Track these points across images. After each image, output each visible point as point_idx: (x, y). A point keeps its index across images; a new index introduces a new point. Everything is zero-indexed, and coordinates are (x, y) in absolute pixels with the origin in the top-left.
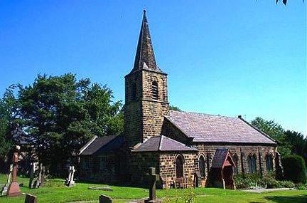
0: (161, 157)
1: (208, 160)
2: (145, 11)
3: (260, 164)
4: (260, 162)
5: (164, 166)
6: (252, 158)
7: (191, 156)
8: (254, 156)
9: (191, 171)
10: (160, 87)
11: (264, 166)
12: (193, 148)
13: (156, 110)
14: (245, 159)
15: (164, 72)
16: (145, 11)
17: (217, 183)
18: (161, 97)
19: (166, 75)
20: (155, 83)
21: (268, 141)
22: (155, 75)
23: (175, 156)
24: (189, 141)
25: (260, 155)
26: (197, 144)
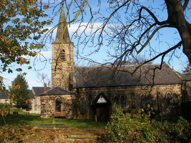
10: (67, 52)
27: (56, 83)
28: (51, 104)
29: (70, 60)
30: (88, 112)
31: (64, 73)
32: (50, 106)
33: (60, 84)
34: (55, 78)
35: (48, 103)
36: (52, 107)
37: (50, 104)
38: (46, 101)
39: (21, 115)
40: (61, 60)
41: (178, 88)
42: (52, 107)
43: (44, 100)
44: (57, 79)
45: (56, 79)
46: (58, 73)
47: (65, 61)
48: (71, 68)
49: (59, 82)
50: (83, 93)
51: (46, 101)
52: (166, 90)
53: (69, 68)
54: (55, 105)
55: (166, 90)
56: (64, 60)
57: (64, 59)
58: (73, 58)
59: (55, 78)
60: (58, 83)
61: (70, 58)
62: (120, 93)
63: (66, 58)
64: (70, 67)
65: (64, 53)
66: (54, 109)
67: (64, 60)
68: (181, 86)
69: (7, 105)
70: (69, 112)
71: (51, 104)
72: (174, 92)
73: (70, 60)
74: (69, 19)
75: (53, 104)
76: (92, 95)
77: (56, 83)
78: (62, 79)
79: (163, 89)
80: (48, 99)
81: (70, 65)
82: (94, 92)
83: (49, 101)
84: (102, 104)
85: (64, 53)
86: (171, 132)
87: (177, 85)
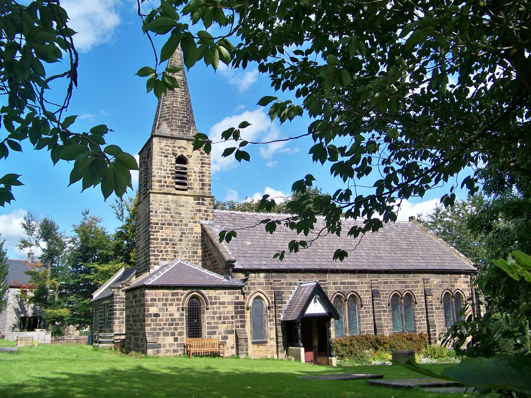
5: (157, 315)
7: (226, 297)
27: (161, 251)
28: (177, 315)
29: (202, 189)
30: (271, 339)
32: (173, 320)
33: (175, 256)
34: (160, 238)
35: (167, 310)
37: (171, 315)
38: (160, 304)
40: (177, 186)
41: (464, 283)
43: (155, 300)
44: (166, 239)
45: (162, 240)
46: (168, 224)
47: (185, 190)
48: (206, 211)
49: (169, 249)
50: (260, 284)
52: (441, 286)
53: (200, 211)
54: (186, 315)
55: (441, 286)
56: (186, 187)
57: (185, 184)
58: (210, 185)
59: (160, 238)
60: (167, 251)
61: (203, 185)
62: (347, 288)
63: (190, 182)
64: (204, 208)
65: (185, 166)
66: (185, 331)
67: (186, 187)
68: (92, 329)
69: (113, 310)
70: (226, 338)
71: (177, 315)
72: (458, 291)
73: (202, 189)
74: (150, 38)
75: (182, 315)
76: (283, 293)
77: (161, 251)
78: (181, 240)
79: (435, 283)
81: (203, 204)
82: (287, 284)
83: (170, 305)
85: (185, 166)
87: (462, 275)
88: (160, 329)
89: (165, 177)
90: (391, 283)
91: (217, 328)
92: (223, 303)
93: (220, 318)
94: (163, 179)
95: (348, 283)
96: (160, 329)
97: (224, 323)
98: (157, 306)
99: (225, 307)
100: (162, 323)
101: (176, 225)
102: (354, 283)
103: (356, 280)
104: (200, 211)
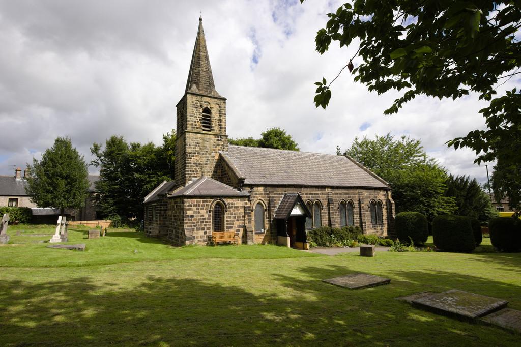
0: (186, 204)
1: (269, 209)
2: (201, 20)
3: (360, 214)
4: (360, 211)
5: (192, 216)
6: (346, 206)
7: (239, 203)
8: (351, 204)
9: (236, 224)
10: (215, 115)
11: (367, 218)
12: (245, 192)
13: (207, 144)
14: (335, 206)
15: (222, 95)
16: (201, 20)
17: (281, 238)
18: (216, 128)
19: (224, 99)
20: (207, 111)
21: (378, 184)
22: (208, 99)
23: (212, 203)
24: (240, 183)
25: (360, 203)
26: (252, 186)
27: (194, 172)
28: (206, 216)
31: (210, 154)
32: (203, 219)
35: (199, 212)
36: (207, 222)
37: (203, 216)
38: (194, 208)
39: (230, 288)
40: (204, 128)
42: (207, 222)
43: (191, 206)
44: (196, 164)
45: (194, 164)
48: (223, 145)
51: (194, 208)
59: (192, 162)
60: (197, 171)
61: (221, 128)
66: (211, 226)
71: (206, 216)
75: (209, 216)
77: (194, 172)
80: (199, 205)
84: (297, 217)
86: (189, 213)
88: (194, 226)
89: (195, 122)
90: (340, 194)
91: (233, 224)
92: (237, 207)
93: (235, 217)
94: (194, 123)
95: (315, 194)
96: (194, 226)
97: (237, 220)
98: (192, 210)
99: (238, 210)
100: (196, 222)
101: (203, 154)
102: (318, 194)
103: (319, 192)
104: (219, 145)
